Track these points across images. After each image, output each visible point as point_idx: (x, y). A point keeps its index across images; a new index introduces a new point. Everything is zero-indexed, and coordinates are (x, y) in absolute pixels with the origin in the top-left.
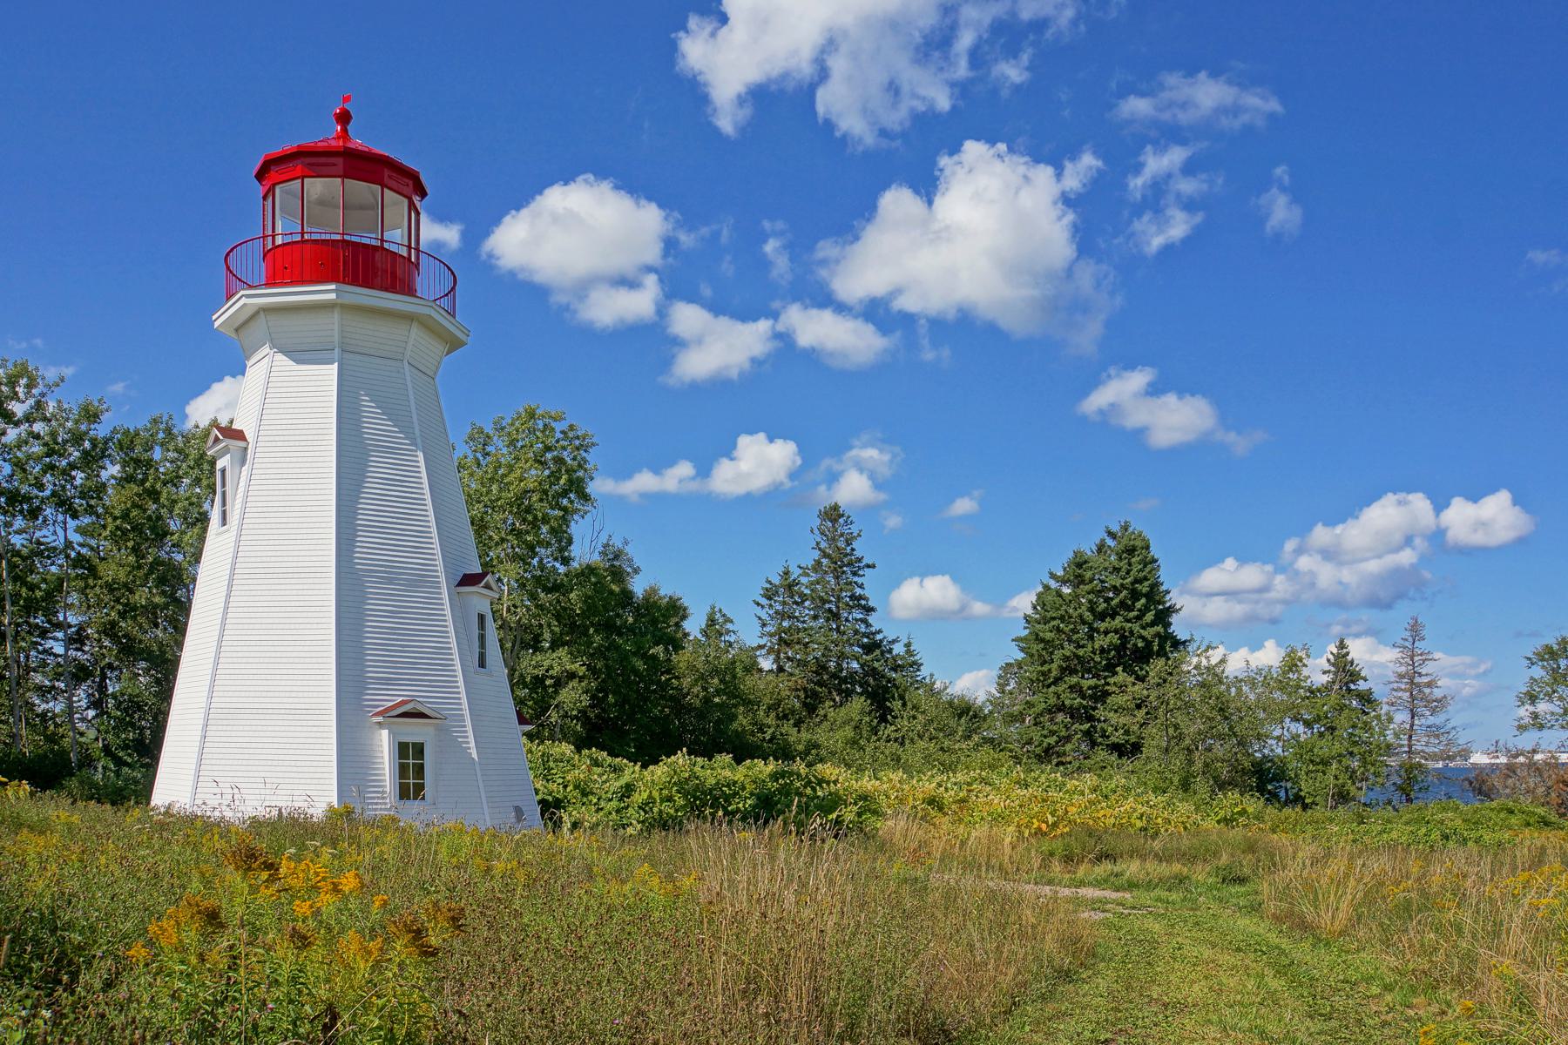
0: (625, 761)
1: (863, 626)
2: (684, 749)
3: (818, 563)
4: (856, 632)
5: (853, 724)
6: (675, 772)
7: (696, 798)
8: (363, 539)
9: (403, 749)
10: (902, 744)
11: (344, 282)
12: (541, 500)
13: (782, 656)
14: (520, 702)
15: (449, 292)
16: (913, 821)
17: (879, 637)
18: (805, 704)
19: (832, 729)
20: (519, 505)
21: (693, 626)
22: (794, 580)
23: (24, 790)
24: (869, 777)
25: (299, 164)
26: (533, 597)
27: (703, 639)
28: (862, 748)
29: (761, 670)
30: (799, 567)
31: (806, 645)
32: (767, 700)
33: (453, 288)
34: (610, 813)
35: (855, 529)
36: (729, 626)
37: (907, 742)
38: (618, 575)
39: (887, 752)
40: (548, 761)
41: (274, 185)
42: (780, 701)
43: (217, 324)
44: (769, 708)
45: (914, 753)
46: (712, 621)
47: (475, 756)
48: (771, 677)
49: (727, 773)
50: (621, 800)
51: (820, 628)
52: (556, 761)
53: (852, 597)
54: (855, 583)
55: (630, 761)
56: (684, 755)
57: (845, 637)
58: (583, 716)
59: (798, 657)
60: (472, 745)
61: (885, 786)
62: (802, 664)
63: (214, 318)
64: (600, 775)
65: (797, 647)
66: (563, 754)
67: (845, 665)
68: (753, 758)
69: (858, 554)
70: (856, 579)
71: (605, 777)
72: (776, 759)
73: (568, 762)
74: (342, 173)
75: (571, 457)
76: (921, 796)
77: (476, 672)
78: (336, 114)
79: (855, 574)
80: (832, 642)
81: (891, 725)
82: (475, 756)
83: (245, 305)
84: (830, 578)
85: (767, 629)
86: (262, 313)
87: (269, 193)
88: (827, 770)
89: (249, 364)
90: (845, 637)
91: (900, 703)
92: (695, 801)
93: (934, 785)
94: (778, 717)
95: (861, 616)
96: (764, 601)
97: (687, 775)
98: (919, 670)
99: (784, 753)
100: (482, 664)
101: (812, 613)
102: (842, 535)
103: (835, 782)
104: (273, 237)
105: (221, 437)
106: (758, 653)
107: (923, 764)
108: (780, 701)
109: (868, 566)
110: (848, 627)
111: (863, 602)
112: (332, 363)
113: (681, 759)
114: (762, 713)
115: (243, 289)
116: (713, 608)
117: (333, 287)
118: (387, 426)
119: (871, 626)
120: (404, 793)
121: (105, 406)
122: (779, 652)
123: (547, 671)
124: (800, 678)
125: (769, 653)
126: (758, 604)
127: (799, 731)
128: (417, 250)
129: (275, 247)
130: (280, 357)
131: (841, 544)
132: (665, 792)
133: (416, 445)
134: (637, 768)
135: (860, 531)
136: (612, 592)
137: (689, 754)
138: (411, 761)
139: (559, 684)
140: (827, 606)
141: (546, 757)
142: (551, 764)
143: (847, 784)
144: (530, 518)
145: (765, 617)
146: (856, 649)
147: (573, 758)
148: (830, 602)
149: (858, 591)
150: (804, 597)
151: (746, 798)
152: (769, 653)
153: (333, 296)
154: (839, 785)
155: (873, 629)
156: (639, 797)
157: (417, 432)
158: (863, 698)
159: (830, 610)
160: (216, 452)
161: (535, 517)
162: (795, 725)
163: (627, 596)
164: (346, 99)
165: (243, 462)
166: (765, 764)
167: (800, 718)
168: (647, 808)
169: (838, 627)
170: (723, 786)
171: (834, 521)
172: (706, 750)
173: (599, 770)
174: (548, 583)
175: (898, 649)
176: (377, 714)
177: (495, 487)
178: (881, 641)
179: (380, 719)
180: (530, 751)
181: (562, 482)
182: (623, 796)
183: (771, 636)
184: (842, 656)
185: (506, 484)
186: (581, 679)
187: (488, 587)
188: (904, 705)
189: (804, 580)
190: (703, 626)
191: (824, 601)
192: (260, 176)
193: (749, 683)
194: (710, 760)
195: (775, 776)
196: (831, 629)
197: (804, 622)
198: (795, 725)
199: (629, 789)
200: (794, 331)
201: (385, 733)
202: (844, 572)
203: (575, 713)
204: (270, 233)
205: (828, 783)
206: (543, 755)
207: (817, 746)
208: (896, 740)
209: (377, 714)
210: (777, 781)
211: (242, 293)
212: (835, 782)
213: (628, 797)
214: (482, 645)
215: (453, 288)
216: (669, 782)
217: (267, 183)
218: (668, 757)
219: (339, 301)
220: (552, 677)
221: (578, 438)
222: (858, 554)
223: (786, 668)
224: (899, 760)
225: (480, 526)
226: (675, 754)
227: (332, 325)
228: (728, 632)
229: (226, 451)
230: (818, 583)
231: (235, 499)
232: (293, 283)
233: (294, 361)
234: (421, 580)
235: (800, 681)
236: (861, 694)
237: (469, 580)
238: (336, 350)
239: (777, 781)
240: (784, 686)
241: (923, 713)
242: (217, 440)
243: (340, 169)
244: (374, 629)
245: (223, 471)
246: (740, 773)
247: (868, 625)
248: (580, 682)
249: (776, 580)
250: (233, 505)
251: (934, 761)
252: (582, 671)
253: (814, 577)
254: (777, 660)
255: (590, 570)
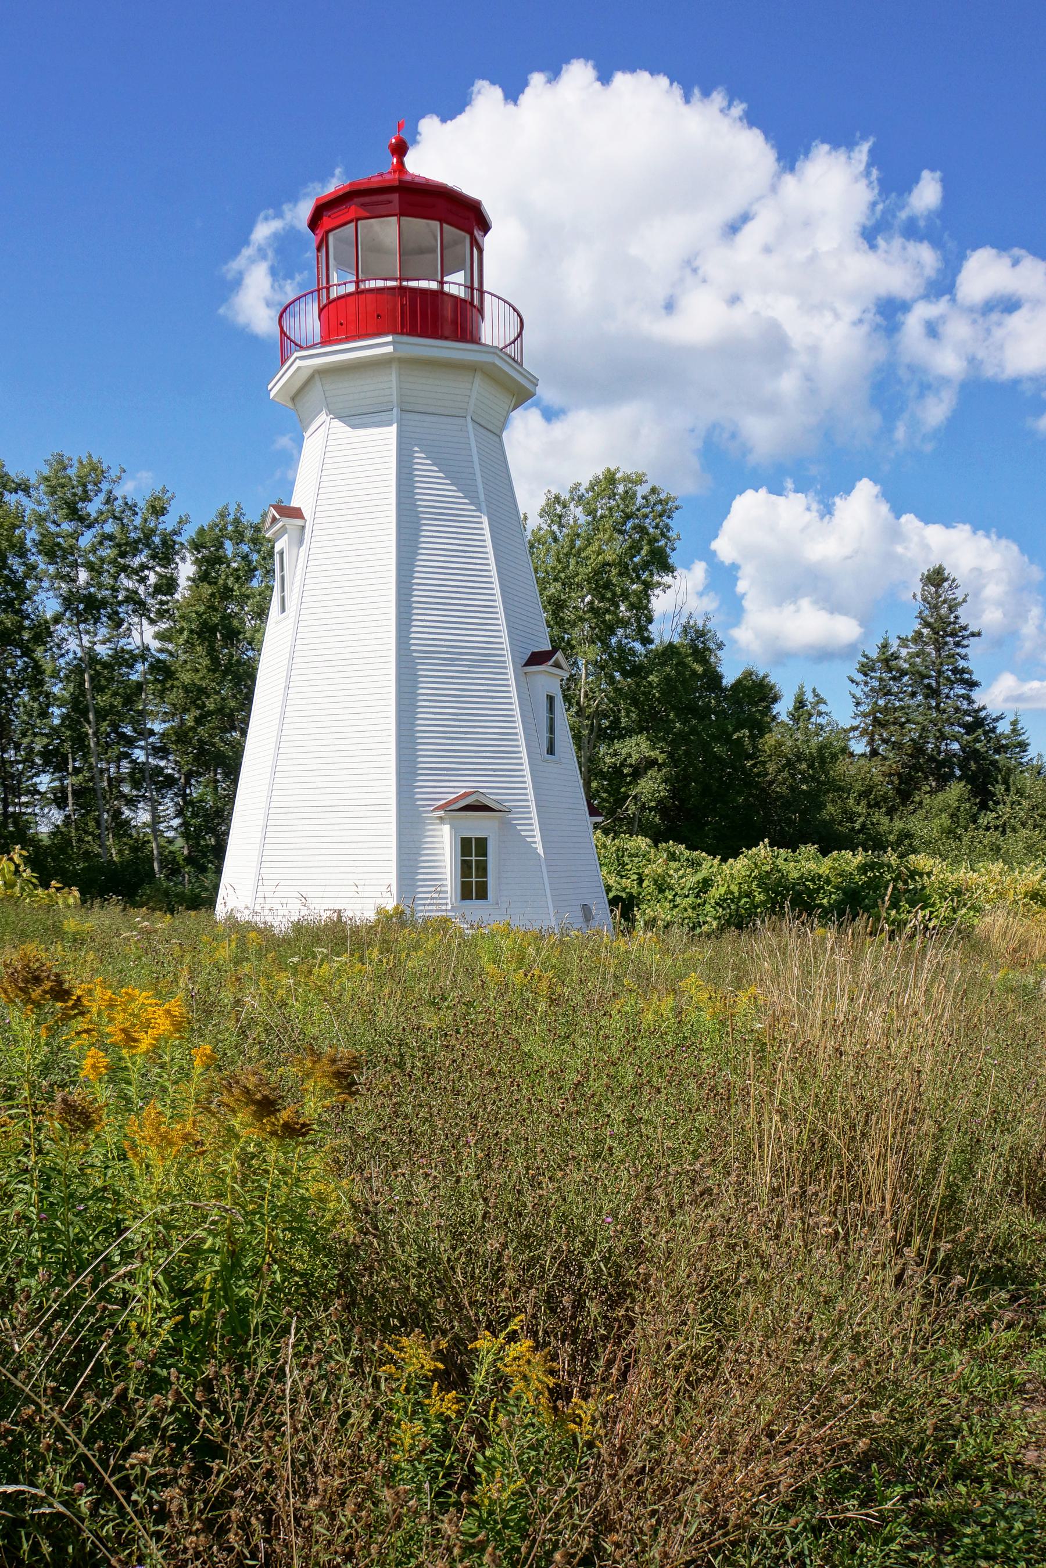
0: (704, 854)
1: (965, 702)
2: (766, 840)
3: (919, 634)
4: (957, 710)
5: (951, 811)
6: (756, 864)
7: (777, 893)
8: (419, 616)
9: (466, 845)
10: (1004, 833)
11: (402, 333)
12: (620, 574)
13: (877, 737)
14: (590, 796)
15: (516, 339)
16: (1014, 918)
17: (983, 714)
18: (898, 791)
19: (926, 818)
20: (597, 581)
21: (783, 709)
22: (892, 654)
23: (75, 897)
24: (966, 868)
25: (353, 209)
26: (612, 680)
27: (791, 723)
28: (959, 838)
29: (852, 755)
30: (899, 638)
31: (902, 725)
32: (858, 787)
33: (520, 334)
34: (686, 910)
35: (959, 594)
36: (822, 708)
37: (1008, 830)
38: (701, 654)
39: (986, 842)
40: (623, 856)
41: (327, 233)
42: (872, 787)
43: (272, 394)
44: (860, 796)
45: (1015, 843)
46: (800, 704)
47: (540, 851)
48: (863, 761)
49: (812, 865)
50: (697, 896)
51: (919, 706)
52: (631, 856)
53: (955, 671)
54: (958, 654)
55: (709, 855)
56: (765, 847)
57: (945, 716)
58: (661, 807)
59: (893, 739)
60: (538, 839)
61: (984, 879)
62: (897, 746)
63: (270, 387)
64: (677, 870)
65: (892, 728)
66: (639, 848)
67: (943, 747)
68: (840, 850)
69: (962, 621)
70: (959, 650)
71: (681, 872)
72: (866, 850)
73: (644, 856)
74: (398, 211)
75: (654, 524)
76: (1023, 891)
77: (544, 761)
78: (391, 145)
79: (958, 644)
80: (931, 722)
81: (992, 811)
82: (540, 851)
83: (299, 368)
84: (930, 649)
85: (861, 708)
86: (317, 377)
87: (322, 244)
88: (921, 861)
89: (306, 435)
90: (945, 716)
91: (1003, 787)
92: (776, 897)
93: (1038, 877)
94: (869, 806)
95: (964, 691)
96: (859, 677)
97: (768, 868)
98: (1025, 751)
99: (878, 844)
100: (551, 751)
101: (910, 689)
102: (945, 602)
103: (929, 874)
104: (328, 289)
105: (278, 516)
106: (851, 735)
107: (1024, 854)
108: (872, 787)
109: (973, 635)
110: (948, 705)
111: (966, 676)
112: (391, 425)
113: (762, 850)
114: (852, 801)
115: (296, 351)
116: (801, 688)
117: (390, 338)
118: (450, 490)
119: (973, 702)
120: (466, 893)
121: (169, 494)
122: (873, 734)
123: (625, 760)
124: (894, 761)
125: (862, 735)
126: (853, 681)
127: (891, 820)
128: (482, 292)
129: (330, 302)
130: (337, 423)
131: (944, 611)
132: (745, 887)
133: (479, 510)
134: (716, 862)
135: (966, 596)
136: (694, 672)
137: (771, 845)
138: (474, 858)
139: (637, 773)
140: (926, 681)
141: (620, 852)
142: (626, 859)
143: (942, 876)
144: (609, 595)
145: (859, 694)
146: (957, 728)
147: (649, 852)
148: (929, 677)
149: (962, 664)
150: (904, 673)
151: (831, 893)
152: (862, 735)
153: (390, 349)
154: (933, 878)
155: (976, 706)
156: (716, 893)
157: (482, 497)
158: (963, 783)
159: (929, 686)
160: (274, 534)
161: (614, 594)
162: (888, 813)
163: (714, 679)
164: (400, 126)
165: (301, 542)
166: (854, 855)
167: (893, 805)
168: (725, 905)
169: (938, 705)
170: (807, 880)
171: (938, 586)
172: (789, 841)
173: (675, 865)
174: (622, 659)
175: (1003, 727)
176: (439, 808)
177: (572, 562)
178: (985, 719)
179: (441, 813)
180: (605, 846)
181: (644, 552)
182: (700, 891)
183: (865, 716)
184: (943, 737)
185: (584, 559)
186: (660, 767)
187: (557, 665)
188: (1007, 790)
189: (904, 652)
190: (791, 708)
191: (924, 677)
192: (314, 223)
193: (842, 767)
194: (794, 851)
195: (863, 869)
196: (930, 708)
197: (901, 700)
198: (888, 813)
199: (706, 884)
200: (879, 299)
201: (446, 828)
202: (946, 643)
203: (653, 804)
204: (325, 285)
205: (921, 875)
206: (618, 850)
207: (909, 835)
208: (996, 828)
209: (439, 808)
210: (865, 873)
211: (297, 354)
212: (929, 874)
213: (705, 893)
214: (551, 729)
215: (520, 334)
216: (749, 876)
217: (320, 232)
218: (749, 848)
219: (397, 355)
220: (631, 766)
221: (660, 502)
222: (962, 621)
223: (880, 751)
224: (999, 849)
225: (557, 606)
226: (757, 845)
227: (389, 383)
228: (820, 714)
229: (283, 530)
230: (918, 656)
231: (293, 584)
232: (348, 339)
233: (349, 426)
234: (485, 660)
235: (894, 766)
236: (960, 779)
237: (537, 659)
238: (395, 410)
239: (865, 873)
240: (876, 770)
241: (1029, 797)
242: (274, 520)
243: (396, 206)
244: (425, 718)
245: (281, 553)
246: (824, 866)
247: (971, 701)
248: (659, 770)
249: (874, 654)
250: (291, 589)
251: (1038, 851)
252: (661, 758)
253: (913, 649)
254: (872, 741)
255: (670, 651)
